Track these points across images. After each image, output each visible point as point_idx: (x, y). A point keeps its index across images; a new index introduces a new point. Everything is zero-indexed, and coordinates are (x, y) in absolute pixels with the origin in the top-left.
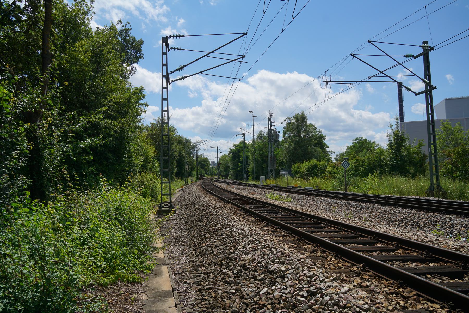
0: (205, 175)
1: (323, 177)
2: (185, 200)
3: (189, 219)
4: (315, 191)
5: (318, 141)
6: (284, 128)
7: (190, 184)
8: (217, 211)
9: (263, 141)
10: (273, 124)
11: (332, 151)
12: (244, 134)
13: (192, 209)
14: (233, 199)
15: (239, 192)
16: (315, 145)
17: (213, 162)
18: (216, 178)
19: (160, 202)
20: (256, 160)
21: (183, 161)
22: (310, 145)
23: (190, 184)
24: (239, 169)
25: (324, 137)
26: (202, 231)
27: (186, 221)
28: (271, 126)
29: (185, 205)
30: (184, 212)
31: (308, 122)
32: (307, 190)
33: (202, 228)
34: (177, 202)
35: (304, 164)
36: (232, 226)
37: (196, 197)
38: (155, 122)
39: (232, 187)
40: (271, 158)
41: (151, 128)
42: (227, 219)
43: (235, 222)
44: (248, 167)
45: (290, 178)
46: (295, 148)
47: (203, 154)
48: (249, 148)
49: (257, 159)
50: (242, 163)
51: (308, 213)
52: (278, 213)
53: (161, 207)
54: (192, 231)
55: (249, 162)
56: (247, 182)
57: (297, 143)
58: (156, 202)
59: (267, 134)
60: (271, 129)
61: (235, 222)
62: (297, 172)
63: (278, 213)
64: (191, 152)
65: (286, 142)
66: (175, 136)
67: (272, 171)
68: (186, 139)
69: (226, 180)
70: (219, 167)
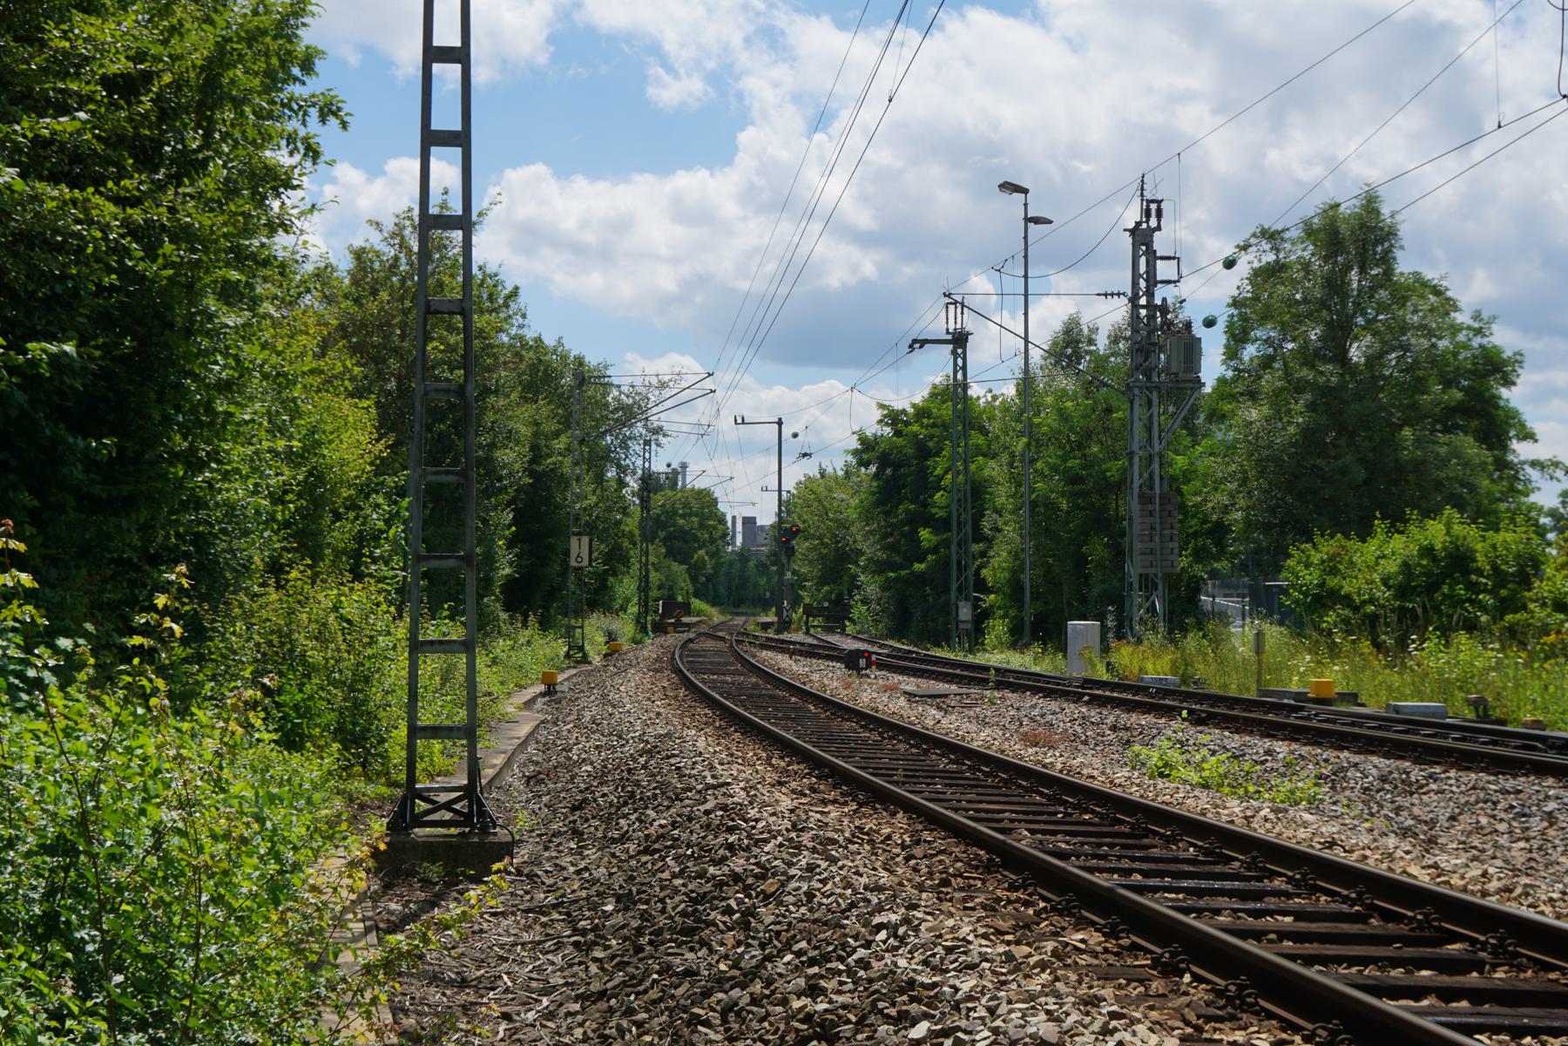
0: (696, 603)
1: (1514, 636)
2: (570, 765)
3: (607, 916)
4: (1250, 704)
5: (1467, 391)
6: (1236, 303)
7: (596, 660)
8: (811, 868)
9: (1090, 386)
10: (1164, 270)
11: (1556, 464)
12: (959, 340)
13: (624, 838)
14: (911, 778)
15: (930, 719)
16: (1450, 418)
17: (749, 522)
18: (765, 626)
19: (403, 777)
20: (1040, 515)
21: (558, 507)
22: (1414, 415)
23: (596, 660)
24: (919, 567)
25: (1505, 363)
26: (707, 1023)
27: (583, 932)
28: (1152, 281)
29: (574, 809)
30: (566, 861)
31: (1405, 265)
32: (1414, 724)
33: (707, 994)
34: (513, 778)
35: (1372, 546)
36: (957, 1008)
37: (649, 753)
38: (375, 240)
39: (886, 689)
40: (1145, 499)
41: (356, 282)
42: (902, 940)
43: (973, 967)
44: (983, 554)
45: (1274, 633)
46: (1310, 439)
47: (684, 466)
48: (994, 428)
49: (1052, 507)
50: (941, 525)
51: (1492, 902)
52: (1259, 895)
53: (402, 820)
54: (630, 1012)
55: (986, 525)
56: (979, 659)
57: (1327, 400)
58: (369, 780)
59: (1115, 340)
60: (1150, 306)
61: (973, 967)
62: (1325, 598)
63: (1259, 895)
64: (608, 450)
65: (1253, 395)
66: (505, 339)
67: (1148, 584)
68: (580, 361)
69: (834, 639)
70: (791, 552)
